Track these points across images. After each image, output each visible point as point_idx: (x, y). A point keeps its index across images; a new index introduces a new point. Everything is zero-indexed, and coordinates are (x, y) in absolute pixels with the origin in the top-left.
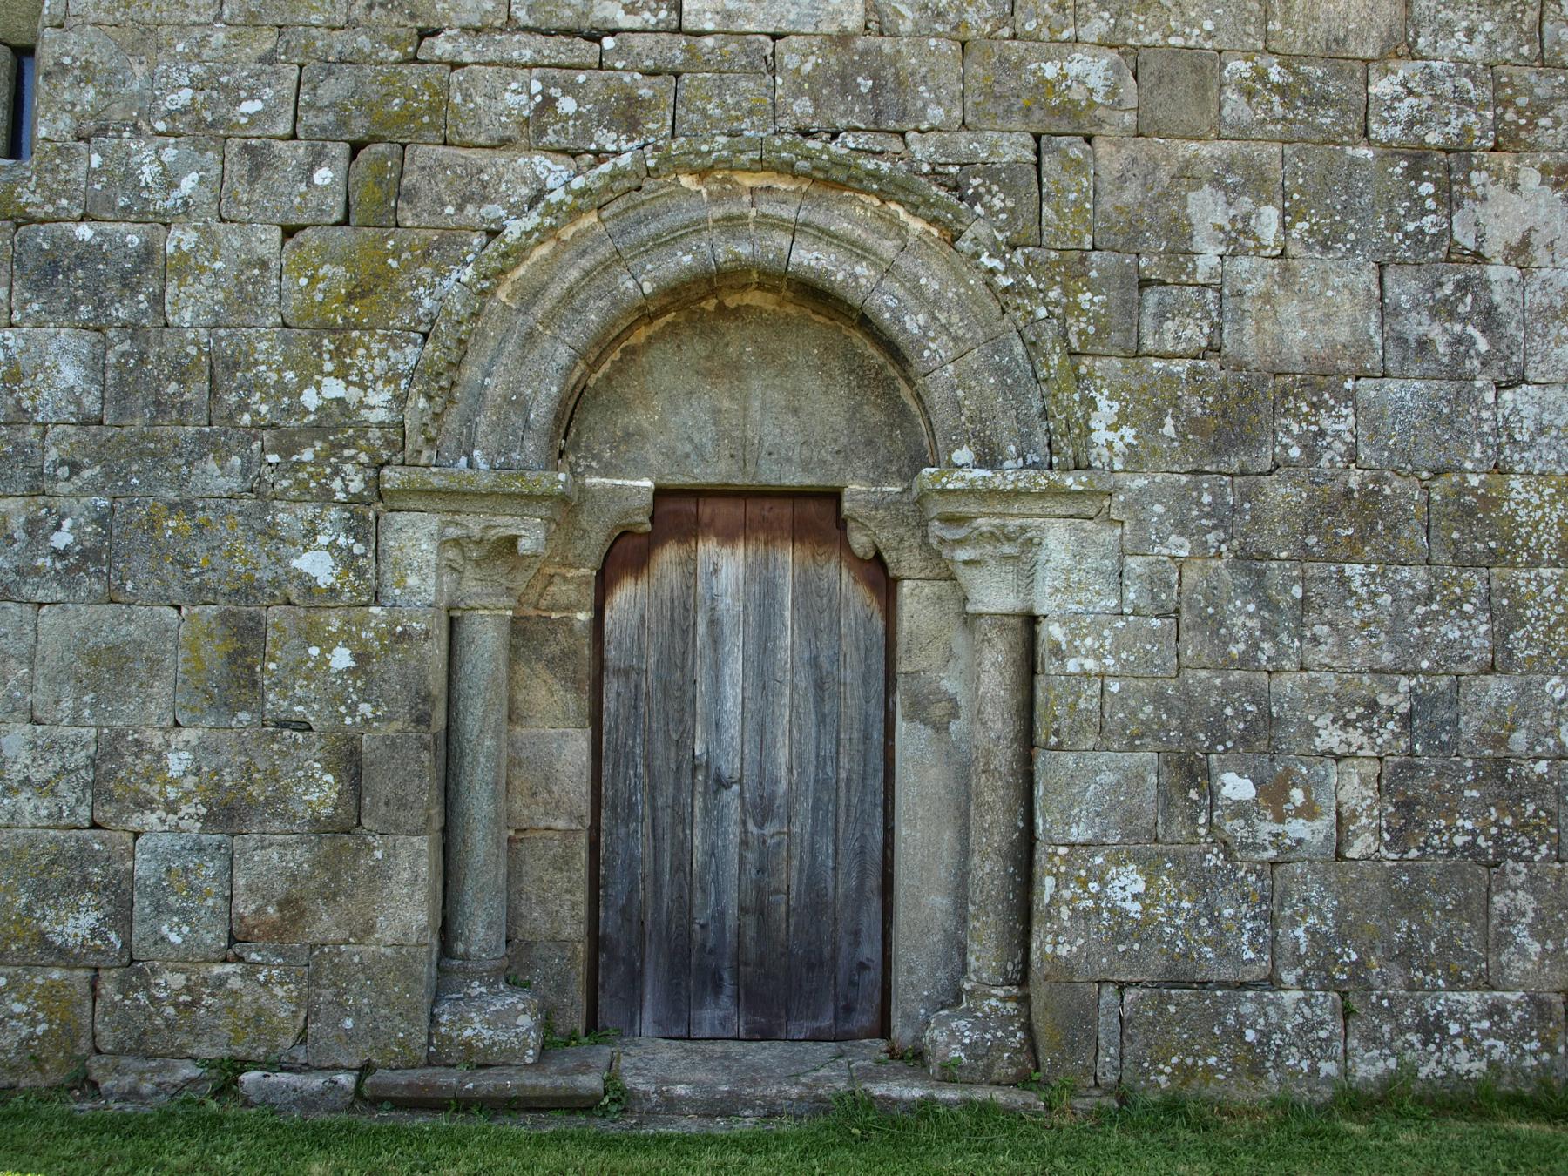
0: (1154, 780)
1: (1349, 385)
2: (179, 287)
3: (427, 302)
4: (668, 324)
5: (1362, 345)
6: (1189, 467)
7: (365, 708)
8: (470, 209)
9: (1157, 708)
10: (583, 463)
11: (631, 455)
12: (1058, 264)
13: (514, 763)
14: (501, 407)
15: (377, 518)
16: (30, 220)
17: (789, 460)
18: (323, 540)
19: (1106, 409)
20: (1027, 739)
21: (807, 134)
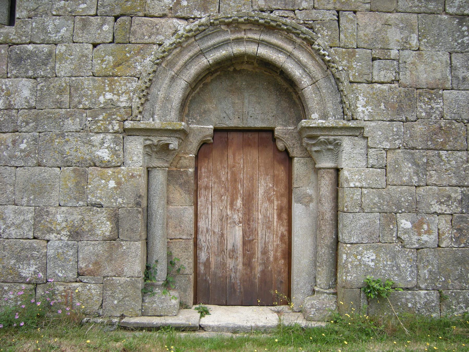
0: (379, 222)
1: (440, 92)
2: (60, 64)
3: (139, 68)
5: (445, 79)
6: (389, 119)
7: (120, 200)
8: (153, 37)
9: (379, 199)
10: (191, 120)
11: (206, 118)
12: (345, 52)
13: (168, 218)
14: (163, 101)
15: (123, 138)
16: (14, 44)
17: (257, 119)
18: (106, 145)
19: (362, 101)
20: (336, 210)
21: (262, 11)
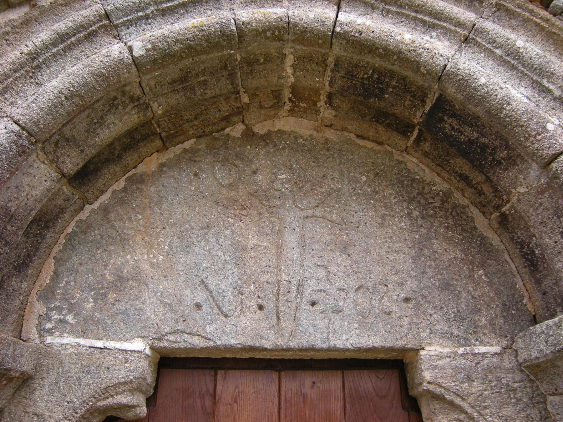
4: (185, 151)
10: (55, 316)
11: (121, 306)
17: (337, 311)
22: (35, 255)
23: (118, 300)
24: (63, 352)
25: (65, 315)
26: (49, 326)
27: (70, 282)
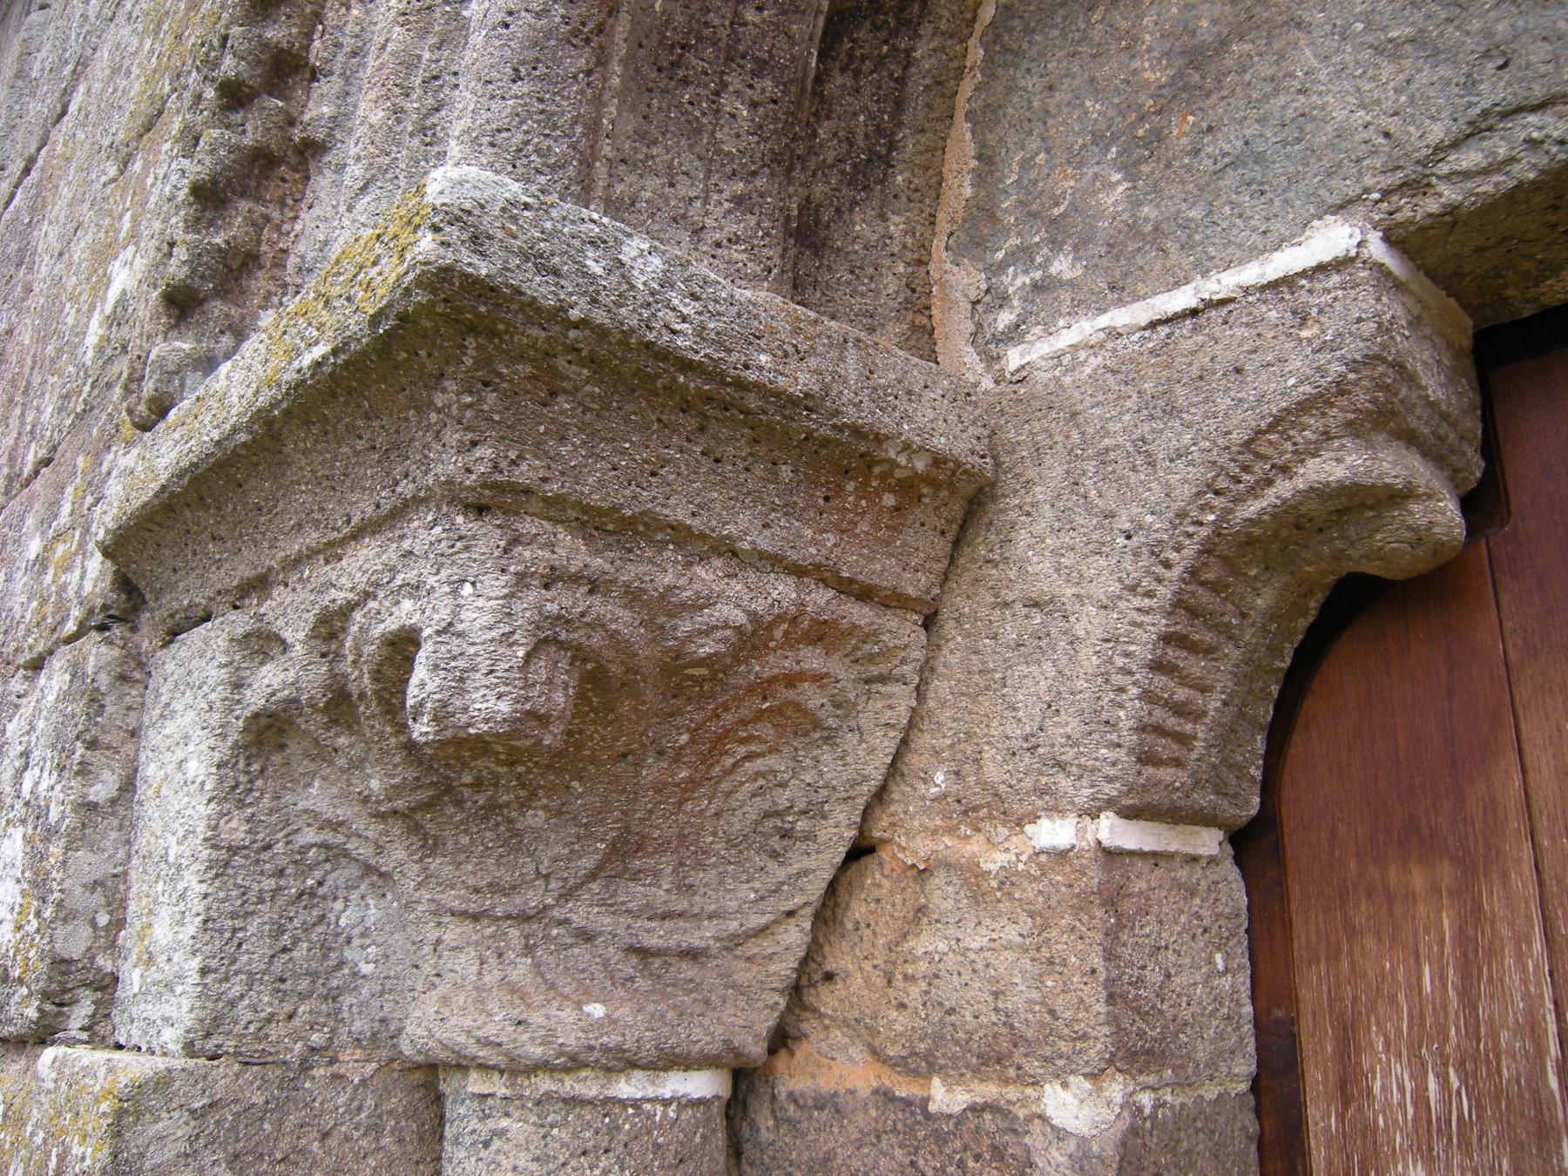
22: (899, 125)
23: (1210, 129)
24: (1067, 380)
25: (1048, 262)
26: (1005, 318)
27: (1032, 158)
